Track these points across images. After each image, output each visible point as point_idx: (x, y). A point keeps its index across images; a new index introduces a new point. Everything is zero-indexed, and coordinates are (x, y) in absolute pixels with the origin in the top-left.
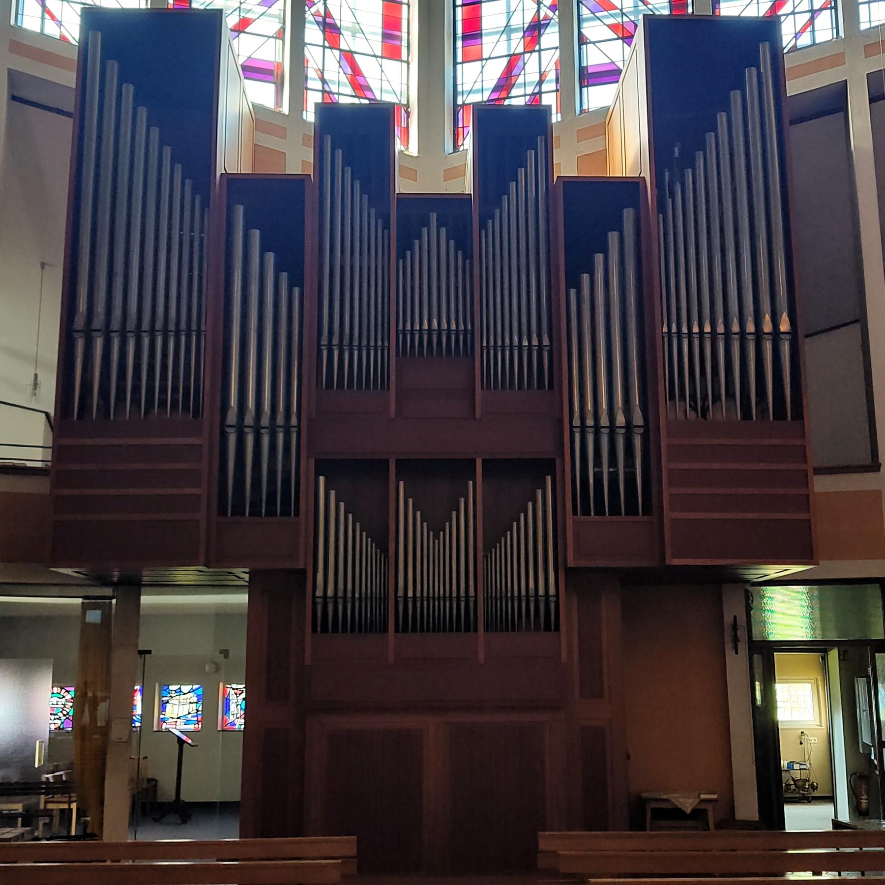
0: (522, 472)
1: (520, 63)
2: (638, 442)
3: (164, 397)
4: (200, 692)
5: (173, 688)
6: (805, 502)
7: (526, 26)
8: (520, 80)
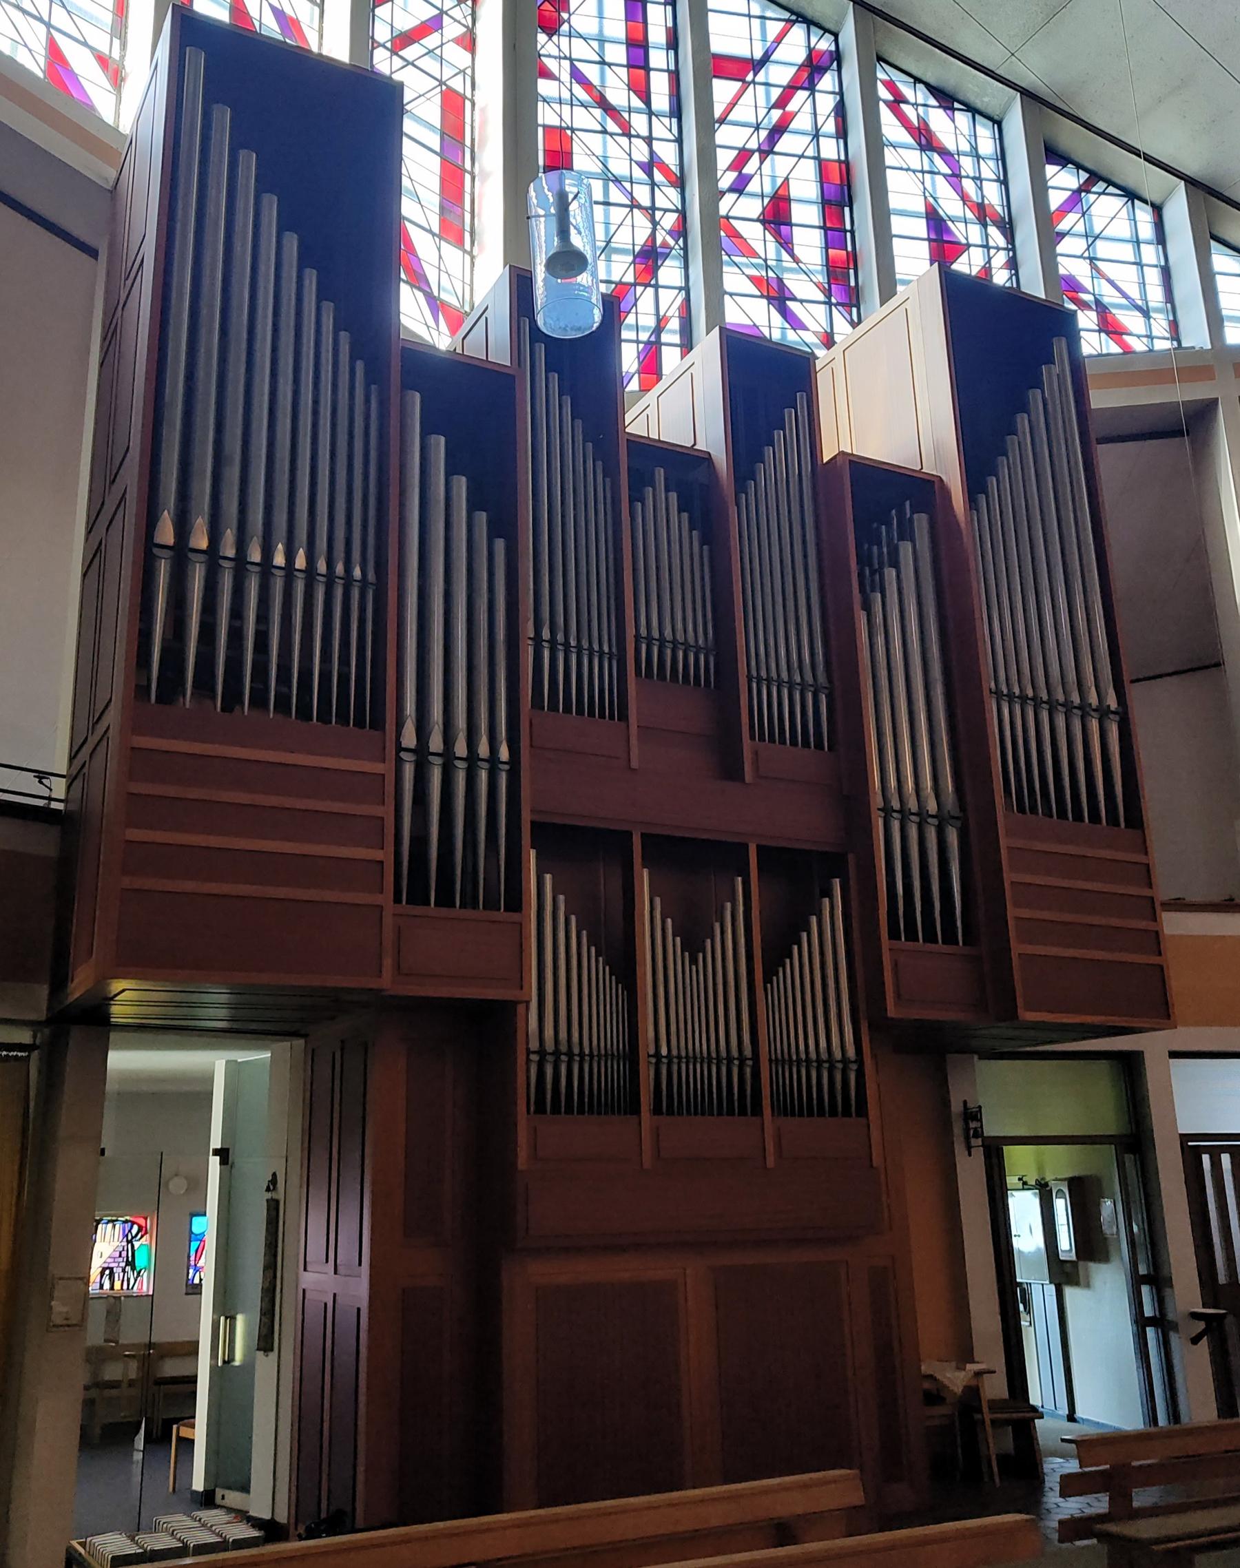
0: (799, 877)
1: (630, 298)
3: (285, 690)
6: (1155, 940)
7: (637, 249)
8: (631, 319)
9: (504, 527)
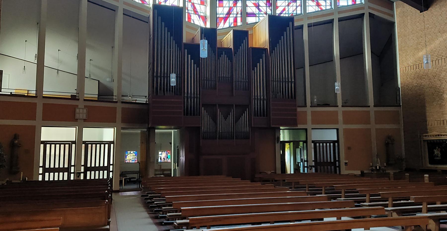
0: (242, 108)
2: (265, 102)
4: (136, 153)
5: (129, 152)
9: (198, 66)
